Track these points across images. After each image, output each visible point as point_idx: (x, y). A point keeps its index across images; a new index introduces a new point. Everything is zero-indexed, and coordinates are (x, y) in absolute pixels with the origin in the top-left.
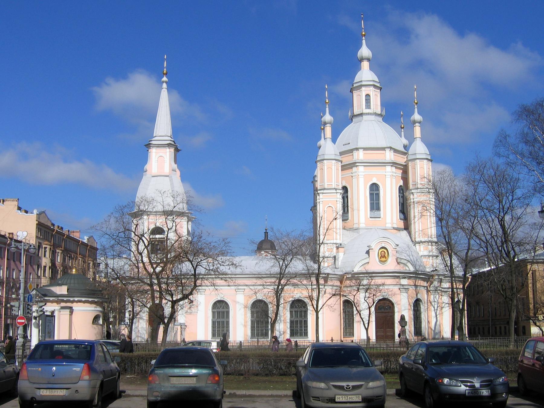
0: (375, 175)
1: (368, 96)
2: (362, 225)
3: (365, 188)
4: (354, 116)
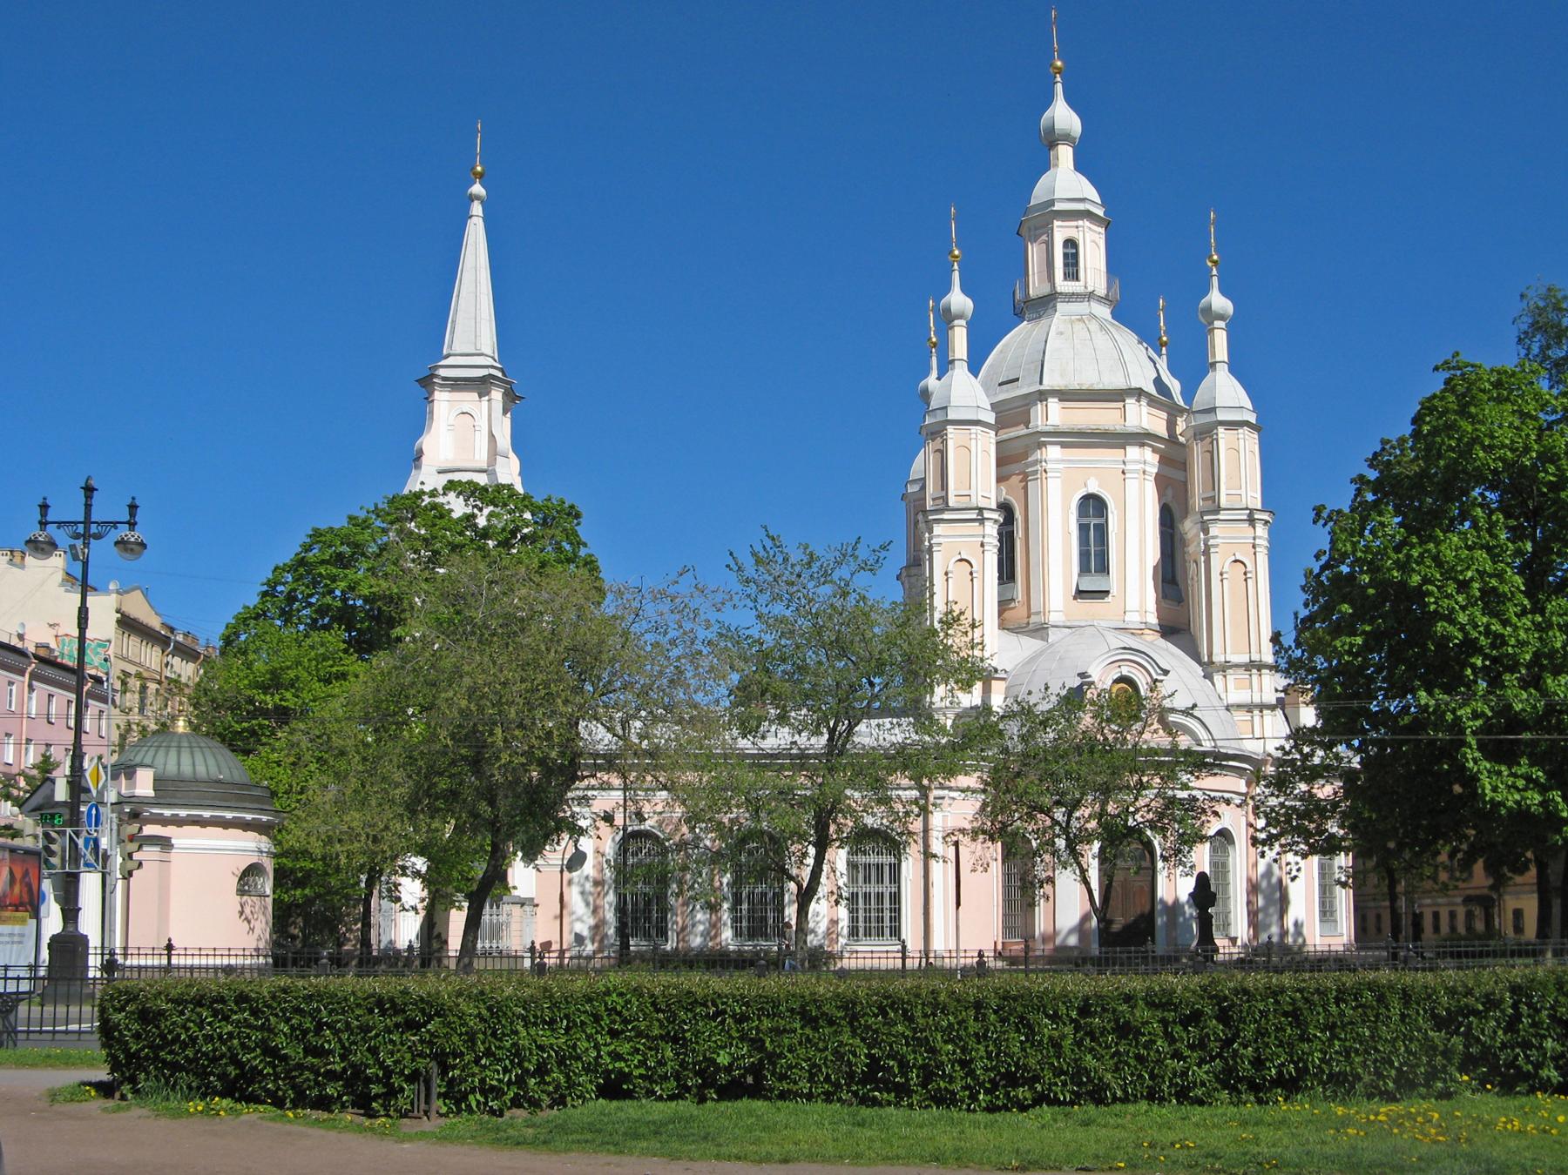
1: (1071, 243)
2: (1053, 618)
3: (1066, 509)
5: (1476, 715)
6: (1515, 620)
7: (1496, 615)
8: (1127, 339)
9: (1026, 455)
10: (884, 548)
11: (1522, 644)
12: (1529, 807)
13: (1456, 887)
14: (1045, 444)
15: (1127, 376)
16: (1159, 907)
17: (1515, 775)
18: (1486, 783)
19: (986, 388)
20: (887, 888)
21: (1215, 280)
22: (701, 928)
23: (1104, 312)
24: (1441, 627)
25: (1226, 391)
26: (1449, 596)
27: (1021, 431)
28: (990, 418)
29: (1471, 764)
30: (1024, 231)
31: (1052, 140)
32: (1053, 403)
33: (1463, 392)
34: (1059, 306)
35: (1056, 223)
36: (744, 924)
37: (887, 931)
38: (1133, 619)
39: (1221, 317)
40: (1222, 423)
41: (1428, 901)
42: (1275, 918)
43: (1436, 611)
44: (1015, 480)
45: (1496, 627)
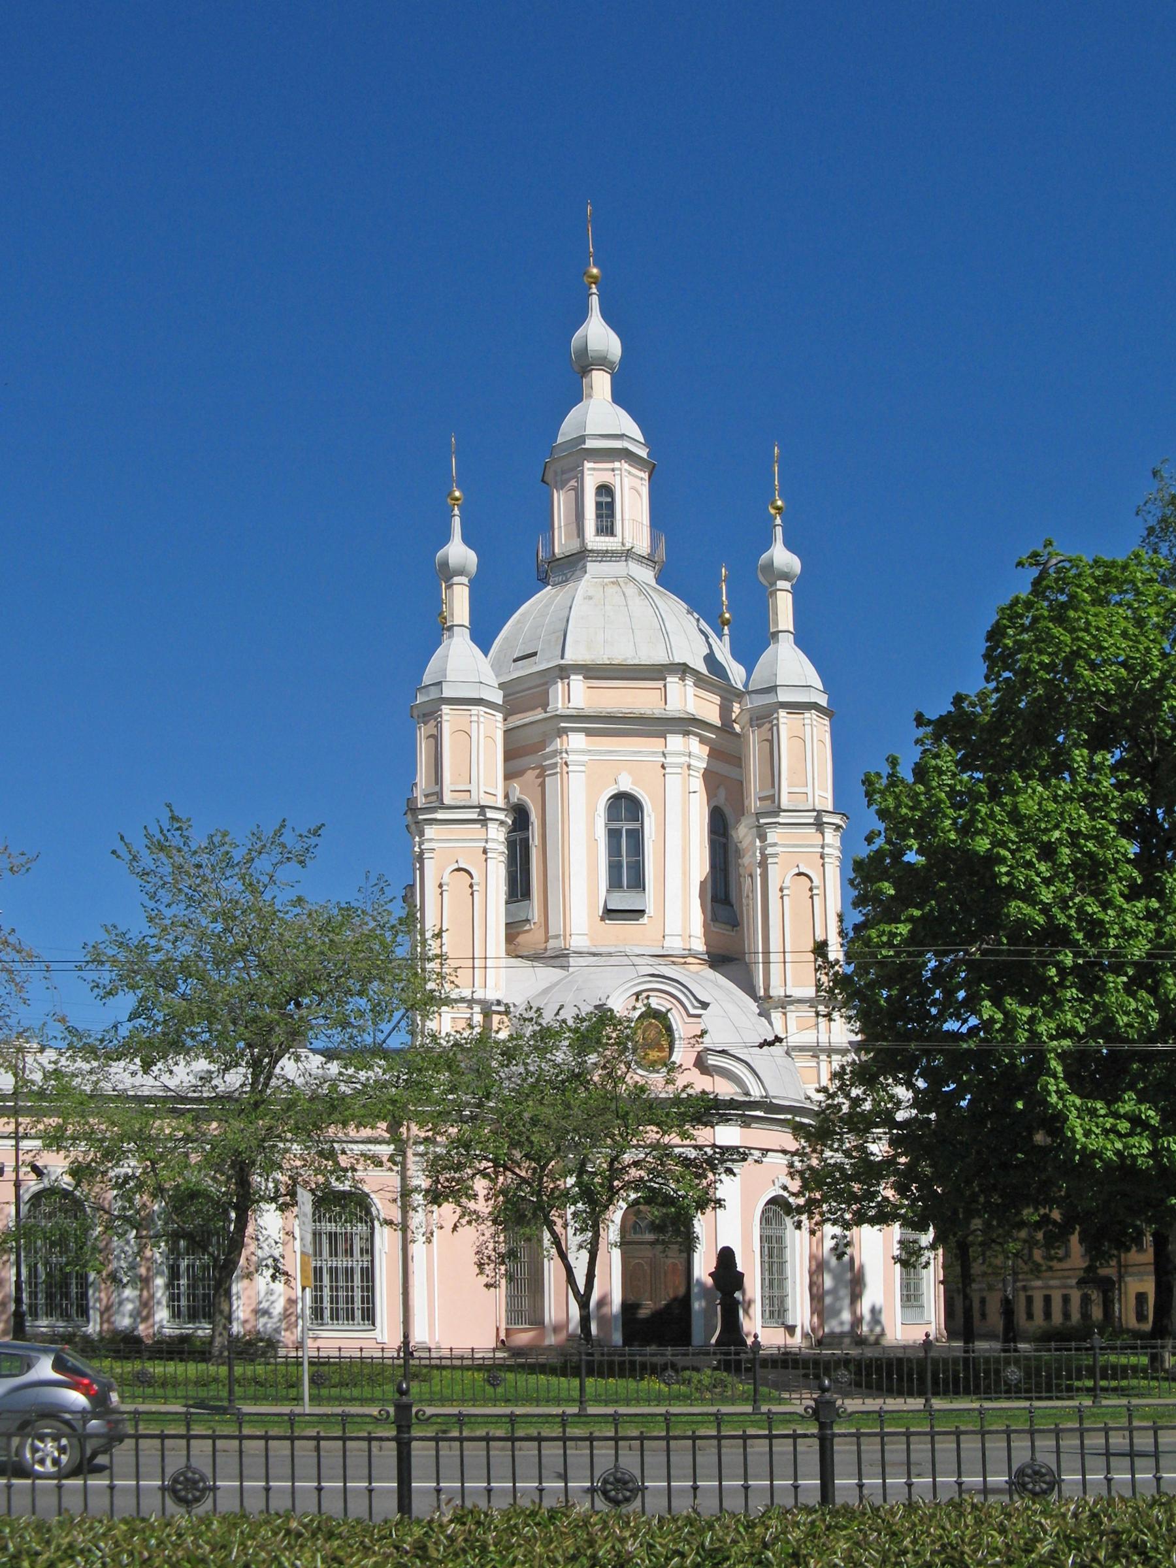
0: (628, 764)
1: (605, 490)
2: (577, 942)
5: (1065, 1032)
6: (1120, 901)
7: (1096, 893)
8: (674, 610)
9: (542, 745)
10: (316, 833)
11: (1130, 934)
12: (1134, 1158)
13: (1050, 1268)
14: (565, 731)
15: (669, 649)
16: (695, 1290)
17: (1116, 1115)
18: (1076, 1126)
19: (497, 668)
20: (357, 1262)
21: (779, 531)
22: (129, 1307)
23: (647, 575)
24: (1017, 908)
25: (791, 667)
26: (1029, 865)
27: (538, 715)
28: (497, 697)
29: (1054, 1099)
30: (549, 477)
31: (586, 364)
32: (577, 681)
33: (1055, 594)
34: (590, 566)
35: (587, 465)
36: (183, 1302)
37: (358, 1314)
38: (674, 944)
39: (786, 576)
40: (784, 705)
41: (1039, 1283)
42: (847, 1301)
43: (1010, 884)
44: (531, 775)
45: (1093, 908)
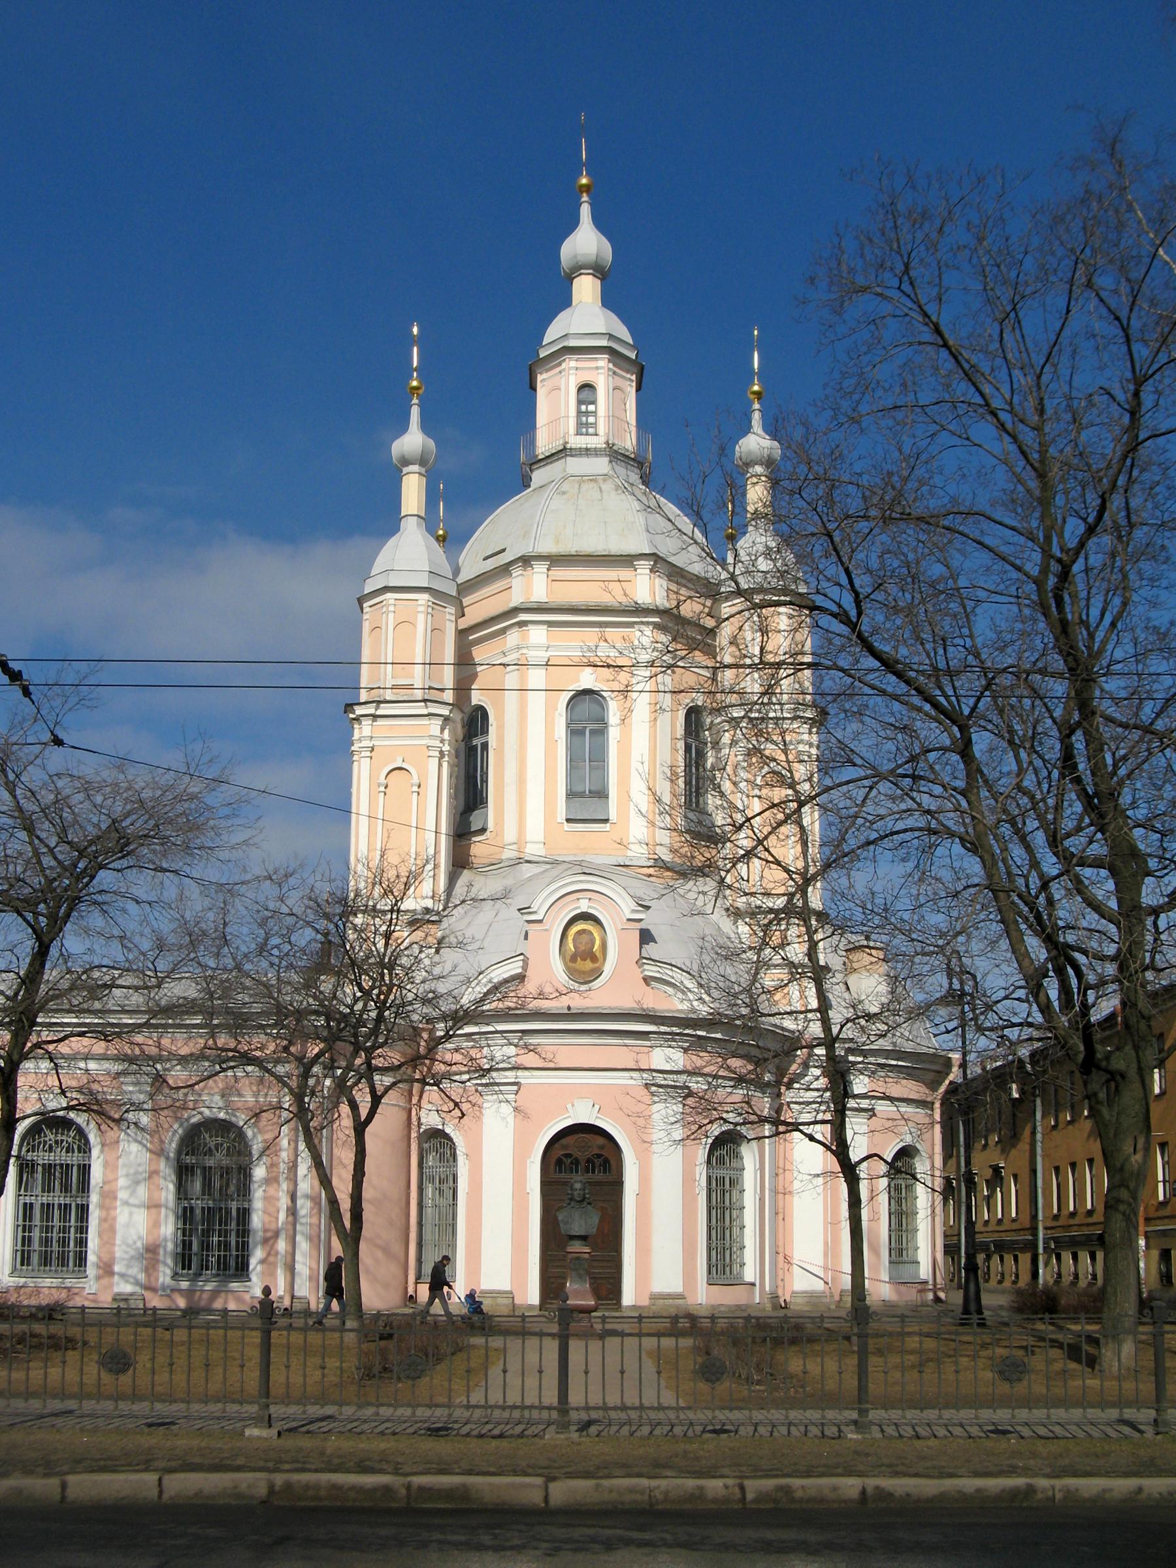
1: (586, 388)
4: (537, 462)
